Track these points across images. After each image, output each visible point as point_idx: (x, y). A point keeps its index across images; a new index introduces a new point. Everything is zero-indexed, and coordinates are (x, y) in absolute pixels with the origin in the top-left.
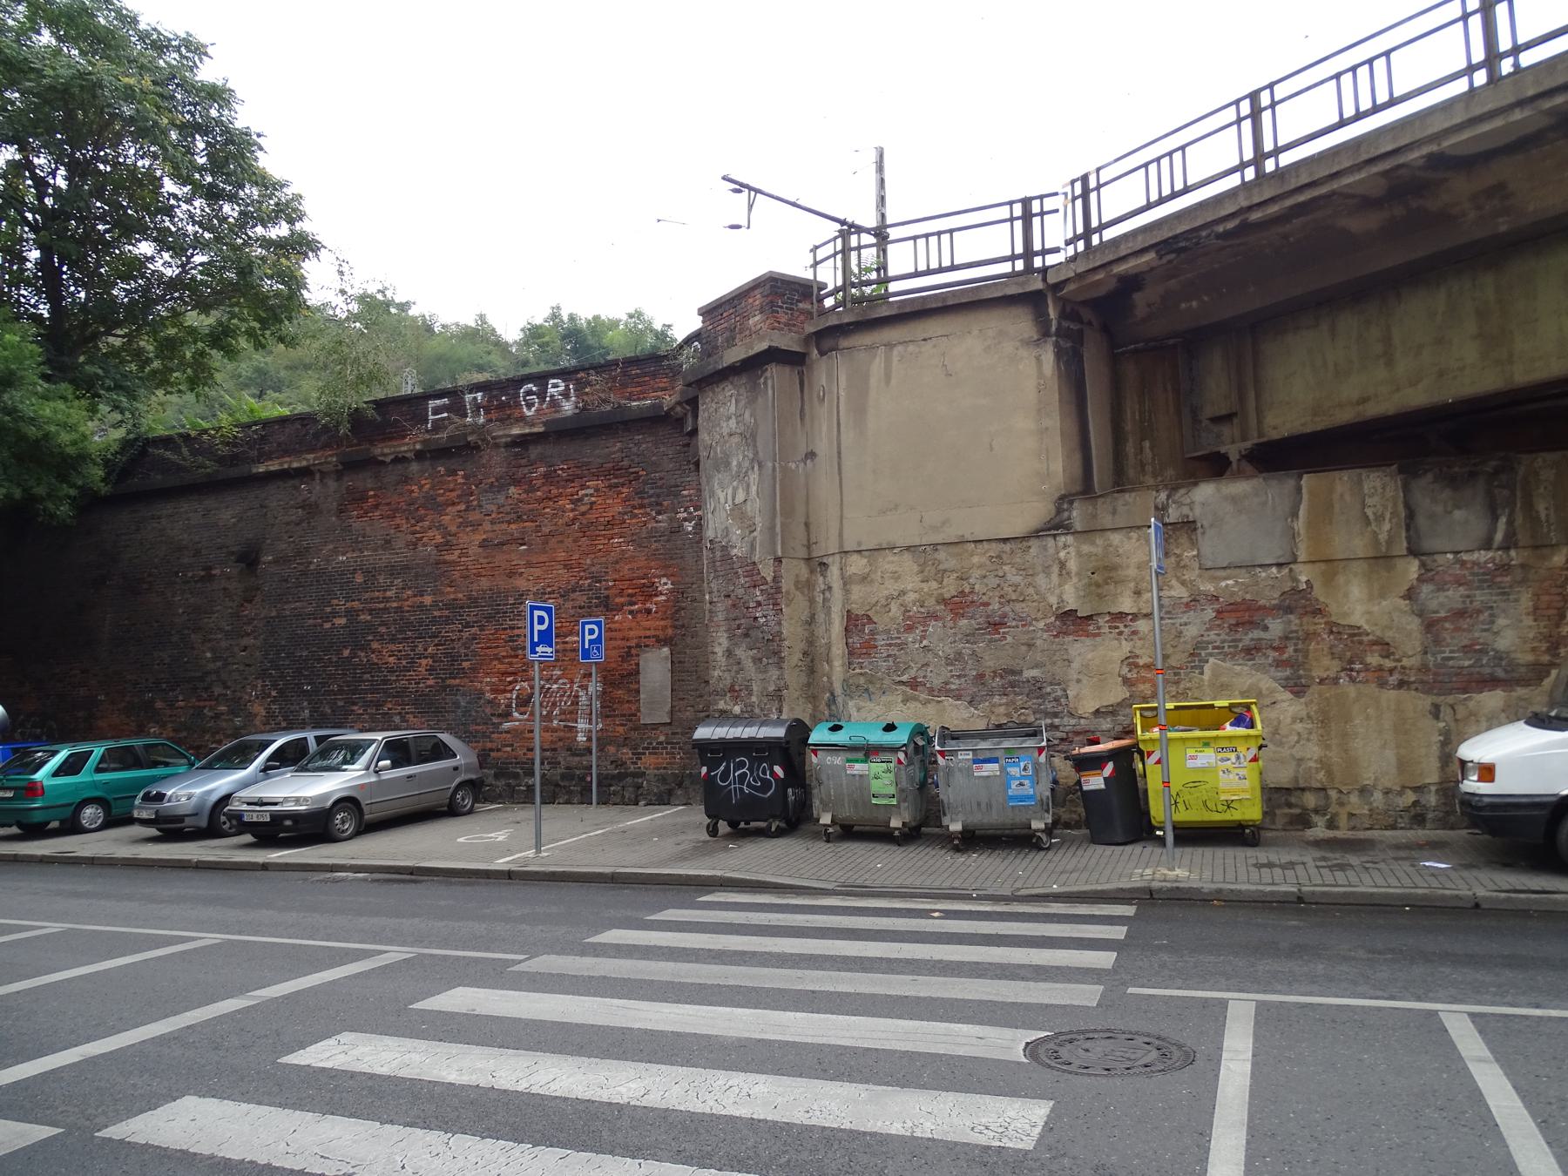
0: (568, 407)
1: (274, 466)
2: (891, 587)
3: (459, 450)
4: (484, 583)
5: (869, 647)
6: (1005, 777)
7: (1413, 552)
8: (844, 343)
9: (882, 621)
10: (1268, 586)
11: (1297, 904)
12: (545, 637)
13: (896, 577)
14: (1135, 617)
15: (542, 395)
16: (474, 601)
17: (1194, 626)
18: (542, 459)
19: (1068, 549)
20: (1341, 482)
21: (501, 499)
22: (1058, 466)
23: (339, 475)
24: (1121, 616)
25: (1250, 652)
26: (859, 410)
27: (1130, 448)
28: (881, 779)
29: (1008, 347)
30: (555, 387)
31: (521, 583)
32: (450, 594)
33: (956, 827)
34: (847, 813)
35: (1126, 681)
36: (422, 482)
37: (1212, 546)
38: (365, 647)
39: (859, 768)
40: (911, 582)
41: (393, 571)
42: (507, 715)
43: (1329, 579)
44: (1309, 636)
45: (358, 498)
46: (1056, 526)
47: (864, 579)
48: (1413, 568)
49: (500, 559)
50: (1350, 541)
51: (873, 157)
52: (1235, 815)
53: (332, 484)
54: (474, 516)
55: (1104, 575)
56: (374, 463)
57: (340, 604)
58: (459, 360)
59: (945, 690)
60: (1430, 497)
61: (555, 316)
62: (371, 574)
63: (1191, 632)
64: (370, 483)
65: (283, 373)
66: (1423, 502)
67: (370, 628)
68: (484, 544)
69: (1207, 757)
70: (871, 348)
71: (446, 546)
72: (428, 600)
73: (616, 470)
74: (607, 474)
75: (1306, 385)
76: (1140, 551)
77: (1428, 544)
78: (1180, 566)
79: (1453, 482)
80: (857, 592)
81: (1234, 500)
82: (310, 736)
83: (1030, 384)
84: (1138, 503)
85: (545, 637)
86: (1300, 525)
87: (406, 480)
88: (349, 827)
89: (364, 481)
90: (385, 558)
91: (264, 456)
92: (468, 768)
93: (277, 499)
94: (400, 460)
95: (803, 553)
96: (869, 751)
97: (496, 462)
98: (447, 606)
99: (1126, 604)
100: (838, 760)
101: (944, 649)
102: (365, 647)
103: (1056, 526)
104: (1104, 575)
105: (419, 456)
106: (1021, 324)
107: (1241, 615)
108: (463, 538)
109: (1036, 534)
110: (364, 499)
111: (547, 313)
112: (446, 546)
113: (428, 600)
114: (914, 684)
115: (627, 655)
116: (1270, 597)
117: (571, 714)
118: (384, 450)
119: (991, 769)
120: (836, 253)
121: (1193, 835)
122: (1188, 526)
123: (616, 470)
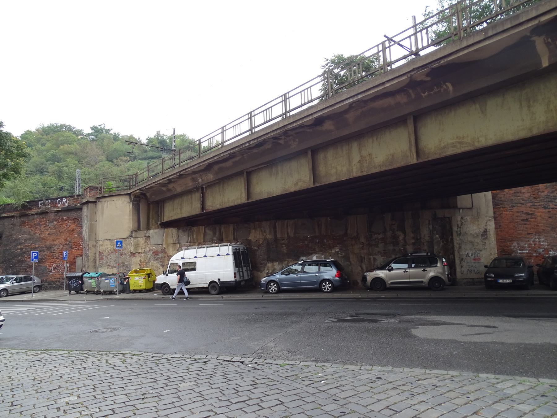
0: (66, 205)
1: (6, 215)
2: (106, 247)
3: (44, 213)
4: (48, 242)
5: (102, 258)
6: (110, 282)
7: (178, 243)
8: (101, 200)
9: (105, 254)
10: (159, 248)
11: (107, 299)
12: (36, 258)
13: (107, 245)
14: (141, 253)
15: (62, 201)
16: (46, 246)
17: (150, 255)
18: (61, 215)
19: (132, 241)
20: (170, 230)
21: (52, 224)
22: (131, 226)
23: (20, 217)
24: (139, 253)
25: (157, 259)
26: (102, 213)
27: (151, 221)
28: (93, 282)
29: (126, 203)
30: (64, 200)
31: (55, 243)
32: (42, 245)
33: (102, 291)
34: (89, 289)
35: (140, 265)
36: (37, 219)
37: (152, 241)
38: (24, 257)
39: (90, 281)
40: (109, 246)
41: (30, 239)
42: (51, 271)
43: (168, 247)
44: (165, 257)
45: (24, 223)
46: (130, 237)
47: (102, 245)
48: (178, 245)
49: (52, 237)
50: (171, 241)
51: (173, 131)
52: (141, 288)
53: (18, 219)
54: (47, 228)
55: (137, 246)
56: (27, 215)
57: (19, 247)
58: (122, 151)
59: (113, 266)
60: (181, 233)
61: (158, 134)
62: (26, 240)
63: (149, 256)
64: (26, 220)
65: (62, 156)
66: (180, 235)
67: (25, 252)
68: (49, 234)
69: (137, 278)
70: (105, 201)
71: (41, 234)
72: (37, 246)
73: (75, 219)
74: (73, 219)
75: (172, 212)
76: (141, 241)
77: (180, 242)
78: (148, 244)
79: (184, 231)
80: (101, 248)
81: (156, 233)
82: (4, 277)
83: (128, 210)
84: (142, 233)
85: (36, 258)
86: (164, 238)
87: (34, 219)
88: (5, 294)
89: (25, 219)
90: (29, 237)
91: (4, 213)
92: (37, 283)
93: (7, 222)
94: (32, 215)
95: (94, 240)
96: (92, 278)
97: (52, 216)
98: (41, 247)
99: (140, 251)
100: (87, 279)
101: (114, 259)
102: (24, 257)
103: (130, 237)
104: (137, 246)
105: (37, 214)
106: (127, 199)
107: (156, 253)
108: (45, 233)
109: (128, 238)
110: (25, 223)
111: (155, 133)
112: (41, 234)
113: (37, 246)
114: (109, 265)
115: (74, 258)
116: (160, 250)
117: (63, 271)
118: (29, 212)
119: (108, 281)
120: (282, 102)
121: (135, 291)
122: (149, 237)
123: (75, 219)
